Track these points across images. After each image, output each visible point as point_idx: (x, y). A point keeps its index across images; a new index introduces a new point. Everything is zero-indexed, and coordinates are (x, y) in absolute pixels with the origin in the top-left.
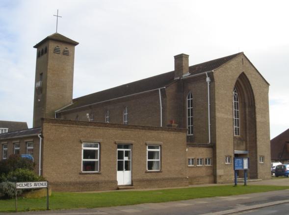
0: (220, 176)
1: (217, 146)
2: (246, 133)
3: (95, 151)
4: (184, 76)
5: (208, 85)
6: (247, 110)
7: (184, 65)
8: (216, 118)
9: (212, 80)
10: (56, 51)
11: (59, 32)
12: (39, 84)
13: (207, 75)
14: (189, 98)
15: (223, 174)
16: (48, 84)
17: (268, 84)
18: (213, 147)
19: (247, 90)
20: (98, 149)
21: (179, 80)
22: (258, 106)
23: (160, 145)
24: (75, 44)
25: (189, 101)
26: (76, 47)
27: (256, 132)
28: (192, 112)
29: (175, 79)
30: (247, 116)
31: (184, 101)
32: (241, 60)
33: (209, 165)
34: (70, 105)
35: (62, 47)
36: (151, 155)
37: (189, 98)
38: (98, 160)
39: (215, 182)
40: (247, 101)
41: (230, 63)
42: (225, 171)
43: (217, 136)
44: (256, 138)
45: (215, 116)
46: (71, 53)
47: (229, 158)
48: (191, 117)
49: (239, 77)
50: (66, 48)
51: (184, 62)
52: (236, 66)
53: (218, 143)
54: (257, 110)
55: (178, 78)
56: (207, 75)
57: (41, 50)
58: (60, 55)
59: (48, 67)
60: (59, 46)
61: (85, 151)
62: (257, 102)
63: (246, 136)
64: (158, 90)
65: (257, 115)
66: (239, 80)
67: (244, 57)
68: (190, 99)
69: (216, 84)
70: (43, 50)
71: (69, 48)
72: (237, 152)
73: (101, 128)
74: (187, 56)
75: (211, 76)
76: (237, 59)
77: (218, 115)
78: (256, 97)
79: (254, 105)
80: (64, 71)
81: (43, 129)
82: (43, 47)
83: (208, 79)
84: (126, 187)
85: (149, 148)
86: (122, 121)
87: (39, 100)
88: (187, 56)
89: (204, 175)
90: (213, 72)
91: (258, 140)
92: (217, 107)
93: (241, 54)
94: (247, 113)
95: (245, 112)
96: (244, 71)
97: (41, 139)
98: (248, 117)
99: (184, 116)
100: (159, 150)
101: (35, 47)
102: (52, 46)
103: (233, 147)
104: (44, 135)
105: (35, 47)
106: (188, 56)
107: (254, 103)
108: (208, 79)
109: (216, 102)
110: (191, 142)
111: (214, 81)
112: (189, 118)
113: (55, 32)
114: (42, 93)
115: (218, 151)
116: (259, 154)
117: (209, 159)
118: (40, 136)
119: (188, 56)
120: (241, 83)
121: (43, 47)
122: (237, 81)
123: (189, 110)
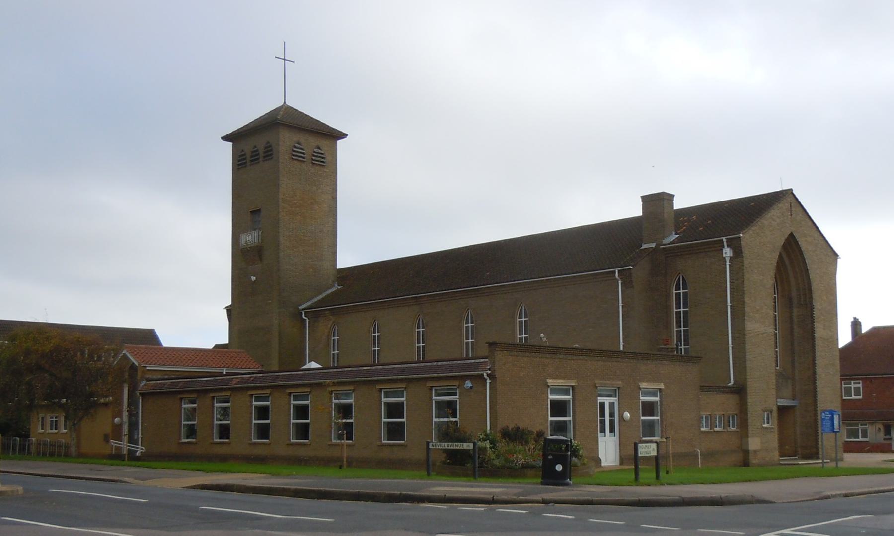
0: (755, 451)
2: (793, 362)
4: (667, 240)
5: (728, 263)
6: (795, 311)
7: (665, 216)
8: (747, 333)
10: (296, 156)
11: (288, 103)
12: (250, 238)
13: (725, 244)
14: (678, 288)
15: (759, 448)
16: (281, 239)
17: (836, 255)
18: (740, 390)
19: (801, 267)
21: (654, 249)
22: (818, 305)
23: (573, 386)
24: (343, 136)
25: (678, 295)
26: (340, 143)
27: (814, 360)
30: (795, 327)
31: (668, 296)
32: (788, 205)
33: (734, 429)
34: (334, 290)
35: (310, 143)
36: (225, 412)
37: (678, 288)
38: (570, 419)
39: (746, 463)
40: (794, 294)
41: (770, 215)
42: (762, 440)
43: (748, 369)
44: (814, 373)
45: (744, 329)
46: (328, 159)
47: (768, 415)
48: (682, 329)
50: (319, 148)
51: (665, 211)
52: (778, 221)
54: (816, 313)
55: (653, 245)
56: (725, 244)
57: (247, 147)
58: (304, 165)
59: (281, 196)
60: (302, 141)
64: (615, 272)
65: (816, 324)
66: (784, 256)
67: (793, 199)
68: (682, 291)
69: (746, 262)
71: (324, 143)
72: (783, 402)
73: (574, 357)
74: (670, 197)
75: (736, 245)
76: (780, 206)
78: (814, 287)
79: (811, 303)
81: (493, 363)
82: (259, 143)
83: (727, 252)
84: (610, 471)
85: (386, 396)
87: (253, 279)
88: (670, 197)
90: (739, 238)
92: (747, 309)
93: (790, 192)
94: (795, 319)
95: (791, 318)
96: (793, 229)
97: (488, 381)
99: (668, 325)
101: (226, 138)
102: (286, 140)
103: (774, 392)
104: (498, 375)
105: (226, 138)
107: (811, 298)
108: (727, 252)
109: (746, 299)
110: (706, 388)
111: (742, 257)
112: (679, 332)
114: (261, 259)
115: (750, 400)
116: (821, 406)
117: (733, 417)
118: (488, 375)
120: (787, 261)
121: (259, 143)
122: (780, 256)
123: (678, 313)
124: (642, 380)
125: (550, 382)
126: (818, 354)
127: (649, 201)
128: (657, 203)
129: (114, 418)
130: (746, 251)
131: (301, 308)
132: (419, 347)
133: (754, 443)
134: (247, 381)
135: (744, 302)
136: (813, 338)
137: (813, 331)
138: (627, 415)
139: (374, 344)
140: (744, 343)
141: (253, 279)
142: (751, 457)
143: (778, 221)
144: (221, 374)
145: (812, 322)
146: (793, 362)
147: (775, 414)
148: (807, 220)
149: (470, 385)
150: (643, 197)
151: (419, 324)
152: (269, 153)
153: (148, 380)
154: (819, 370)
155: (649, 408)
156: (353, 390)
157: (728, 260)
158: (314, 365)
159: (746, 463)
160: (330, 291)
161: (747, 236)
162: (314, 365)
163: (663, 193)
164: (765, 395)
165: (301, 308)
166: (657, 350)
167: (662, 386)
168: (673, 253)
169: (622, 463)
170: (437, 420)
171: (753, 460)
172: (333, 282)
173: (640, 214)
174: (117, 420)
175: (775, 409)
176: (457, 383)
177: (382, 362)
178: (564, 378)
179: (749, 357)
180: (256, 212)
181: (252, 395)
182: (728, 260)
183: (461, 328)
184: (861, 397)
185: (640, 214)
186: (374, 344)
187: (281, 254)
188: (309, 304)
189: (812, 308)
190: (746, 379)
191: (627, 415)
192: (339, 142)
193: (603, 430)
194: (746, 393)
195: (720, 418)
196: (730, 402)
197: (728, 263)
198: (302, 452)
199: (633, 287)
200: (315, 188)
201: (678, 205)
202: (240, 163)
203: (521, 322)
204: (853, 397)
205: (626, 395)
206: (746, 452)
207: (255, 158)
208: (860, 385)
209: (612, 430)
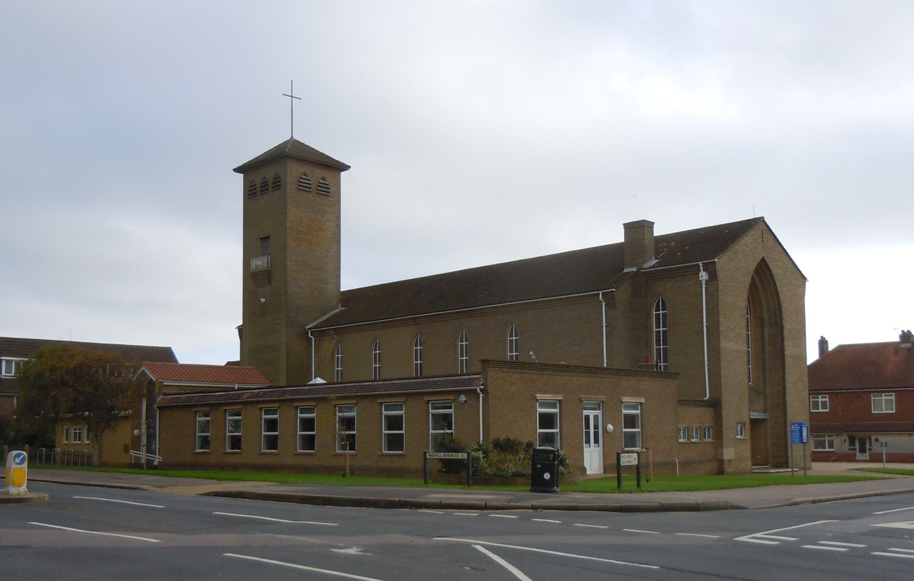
0: (730, 461)
1: (724, 405)
2: (764, 377)
3: (400, 418)
4: (646, 266)
5: (704, 286)
6: (767, 331)
8: (722, 351)
9: (713, 276)
10: (303, 186)
11: (296, 137)
12: (259, 263)
16: (289, 263)
17: (804, 279)
18: (715, 404)
20: (557, 410)
22: (787, 325)
24: (346, 168)
25: (658, 316)
28: (664, 338)
29: (626, 270)
30: (766, 345)
31: (648, 317)
32: (759, 232)
33: (709, 440)
34: (337, 311)
35: (315, 175)
36: (272, 425)
39: (721, 472)
40: (766, 315)
42: (736, 450)
44: (784, 388)
46: (333, 189)
49: (756, 270)
50: (324, 179)
51: (646, 237)
52: (751, 247)
53: (725, 397)
54: (786, 332)
55: (635, 269)
57: (258, 178)
59: (288, 224)
60: (308, 172)
61: (541, 415)
62: (785, 316)
63: (765, 383)
65: (786, 343)
66: (756, 279)
68: (661, 312)
69: (721, 285)
70: (264, 185)
71: (328, 174)
72: (755, 415)
77: (725, 344)
78: (784, 308)
79: (781, 323)
80: (321, 234)
81: (486, 379)
82: (269, 174)
83: (703, 276)
84: (595, 479)
85: (386, 410)
86: (506, 355)
87: (263, 300)
89: (846, 438)
91: (787, 392)
92: (722, 329)
95: (763, 337)
96: (764, 254)
97: (481, 395)
98: (768, 348)
99: (648, 343)
100: (557, 410)
101: (238, 170)
102: (293, 172)
103: (747, 405)
104: (490, 389)
105: (238, 170)
106: (653, 223)
107: (781, 318)
108: (703, 276)
109: (721, 320)
112: (658, 350)
113: (286, 137)
114: (270, 282)
115: (724, 414)
117: (709, 429)
119: (653, 223)
121: (269, 174)
124: (625, 394)
125: (626, 399)
126: (787, 371)
127: (630, 228)
128: (638, 230)
129: (133, 429)
130: (720, 275)
131: (307, 327)
132: (462, 361)
133: (728, 454)
134: (257, 395)
135: (719, 322)
136: (783, 355)
137: (782, 349)
138: (610, 427)
139: (375, 361)
140: (719, 360)
141: (263, 300)
142: (726, 465)
143: (751, 247)
144: (233, 389)
145: (783, 341)
146: (764, 377)
147: (748, 426)
148: (778, 246)
149: (464, 399)
150: (625, 225)
151: (658, 306)
152: (277, 184)
153: (165, 394)
154: (788, 385)
155: (630, 421)
156: (356, 404)
157: (704, 283)
158: (319, 381)
159: (721, 472)
160: (334, 312)
161: (722, 260)
162: (319, 381)
163: (644, 221)
164: (738, 409)
165: (307, 327)
166: (640, 368)
167: (643, 400)
168: (652, 276)
169: (605, 472)
170: (434, 432)
171: (728, 469)
172: (337, 303)
173: (622, 240)
174: (136, 432)
175: (748, 421)
176: (452, 397)
177: (424, 374)
178: (551, 393)
179: (723, 372)
180: (265, 239)
181: (382, 403)
182: (704, 283)
183: (456, 347)
184: (827, 410)
185: (622, 240)
186: (375, 361)
187: (289, 278)
188: (315, 323)
189: (782, 328)
190: (720, 393)
191: (610, 427)
192: (342, 173)
193: (588, 441)
194: (721, 407)
195: (684, 430)
196: (706, 415)
197: (704, 286)
198: (308, 462)
199: (615, 308)
200: (320, 216)
201: (658, 232)
202: (250, 193)
203: (462, 346)
204: (821, 410)
205: (609, 408)
206: (721, 462)
207: (264, 188)
208: (827, 400)
209: (596, 441)
